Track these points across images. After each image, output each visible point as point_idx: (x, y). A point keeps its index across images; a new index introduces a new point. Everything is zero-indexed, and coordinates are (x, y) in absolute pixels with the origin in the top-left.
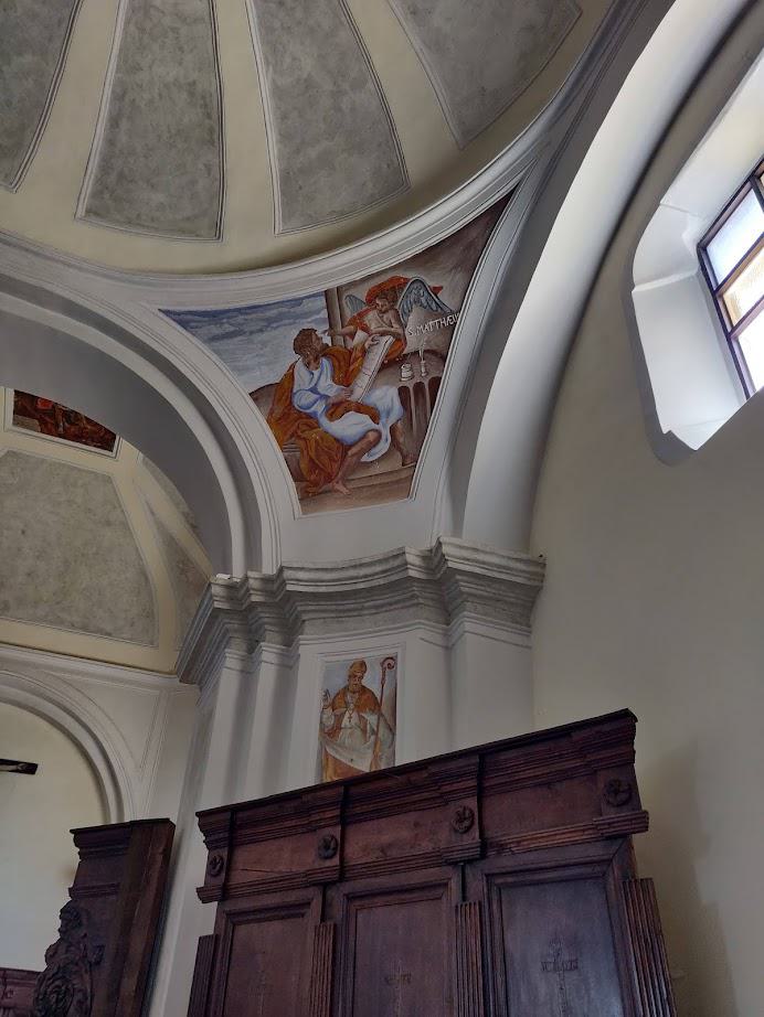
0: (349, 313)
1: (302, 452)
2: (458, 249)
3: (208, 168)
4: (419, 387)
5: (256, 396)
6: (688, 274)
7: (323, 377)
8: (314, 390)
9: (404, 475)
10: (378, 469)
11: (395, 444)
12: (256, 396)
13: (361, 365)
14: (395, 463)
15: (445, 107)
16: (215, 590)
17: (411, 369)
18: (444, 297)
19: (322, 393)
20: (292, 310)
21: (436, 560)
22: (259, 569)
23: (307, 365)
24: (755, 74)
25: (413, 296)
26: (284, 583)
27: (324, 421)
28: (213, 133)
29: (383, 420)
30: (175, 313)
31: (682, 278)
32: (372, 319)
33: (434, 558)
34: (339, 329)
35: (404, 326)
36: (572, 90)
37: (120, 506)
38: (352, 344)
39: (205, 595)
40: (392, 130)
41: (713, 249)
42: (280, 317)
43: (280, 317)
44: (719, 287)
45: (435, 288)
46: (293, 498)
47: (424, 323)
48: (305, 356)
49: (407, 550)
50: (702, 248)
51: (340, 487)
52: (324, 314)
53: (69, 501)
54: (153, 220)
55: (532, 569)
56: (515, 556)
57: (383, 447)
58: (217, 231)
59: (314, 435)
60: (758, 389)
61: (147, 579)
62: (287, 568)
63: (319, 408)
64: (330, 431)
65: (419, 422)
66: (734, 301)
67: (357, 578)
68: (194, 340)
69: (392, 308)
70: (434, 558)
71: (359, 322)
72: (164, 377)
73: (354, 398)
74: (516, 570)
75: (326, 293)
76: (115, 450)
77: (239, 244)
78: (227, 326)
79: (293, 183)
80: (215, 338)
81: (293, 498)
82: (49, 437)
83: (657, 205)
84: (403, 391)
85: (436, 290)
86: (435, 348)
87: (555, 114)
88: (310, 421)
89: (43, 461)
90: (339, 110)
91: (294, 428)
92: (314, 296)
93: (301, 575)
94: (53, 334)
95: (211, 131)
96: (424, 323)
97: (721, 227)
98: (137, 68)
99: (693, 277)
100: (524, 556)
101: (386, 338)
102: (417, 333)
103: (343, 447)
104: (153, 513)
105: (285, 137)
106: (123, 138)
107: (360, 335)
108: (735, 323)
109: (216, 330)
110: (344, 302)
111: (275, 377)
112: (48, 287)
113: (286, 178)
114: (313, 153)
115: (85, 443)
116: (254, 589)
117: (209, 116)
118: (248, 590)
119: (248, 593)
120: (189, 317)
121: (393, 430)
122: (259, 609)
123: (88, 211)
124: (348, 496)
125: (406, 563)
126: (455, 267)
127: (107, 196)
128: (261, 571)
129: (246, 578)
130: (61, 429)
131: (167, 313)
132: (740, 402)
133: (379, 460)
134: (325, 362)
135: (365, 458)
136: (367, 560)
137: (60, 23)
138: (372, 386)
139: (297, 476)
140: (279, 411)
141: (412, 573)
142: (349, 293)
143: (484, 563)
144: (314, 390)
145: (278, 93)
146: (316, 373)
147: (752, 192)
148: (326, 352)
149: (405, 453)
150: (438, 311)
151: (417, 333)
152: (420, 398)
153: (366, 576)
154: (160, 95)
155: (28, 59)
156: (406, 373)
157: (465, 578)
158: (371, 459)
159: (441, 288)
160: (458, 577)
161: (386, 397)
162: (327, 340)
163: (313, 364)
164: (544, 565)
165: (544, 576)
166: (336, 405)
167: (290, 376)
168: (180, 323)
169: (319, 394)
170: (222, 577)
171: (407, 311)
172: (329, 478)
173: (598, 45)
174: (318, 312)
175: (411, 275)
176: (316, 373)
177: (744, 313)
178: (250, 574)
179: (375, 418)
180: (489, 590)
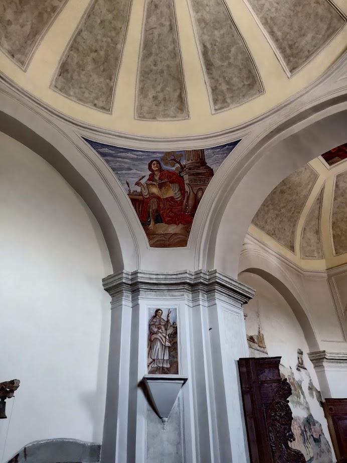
94: (318, 124)
123: (291, 71)
127: (291, 59)
137: (231, 28)
155: (233, 50)
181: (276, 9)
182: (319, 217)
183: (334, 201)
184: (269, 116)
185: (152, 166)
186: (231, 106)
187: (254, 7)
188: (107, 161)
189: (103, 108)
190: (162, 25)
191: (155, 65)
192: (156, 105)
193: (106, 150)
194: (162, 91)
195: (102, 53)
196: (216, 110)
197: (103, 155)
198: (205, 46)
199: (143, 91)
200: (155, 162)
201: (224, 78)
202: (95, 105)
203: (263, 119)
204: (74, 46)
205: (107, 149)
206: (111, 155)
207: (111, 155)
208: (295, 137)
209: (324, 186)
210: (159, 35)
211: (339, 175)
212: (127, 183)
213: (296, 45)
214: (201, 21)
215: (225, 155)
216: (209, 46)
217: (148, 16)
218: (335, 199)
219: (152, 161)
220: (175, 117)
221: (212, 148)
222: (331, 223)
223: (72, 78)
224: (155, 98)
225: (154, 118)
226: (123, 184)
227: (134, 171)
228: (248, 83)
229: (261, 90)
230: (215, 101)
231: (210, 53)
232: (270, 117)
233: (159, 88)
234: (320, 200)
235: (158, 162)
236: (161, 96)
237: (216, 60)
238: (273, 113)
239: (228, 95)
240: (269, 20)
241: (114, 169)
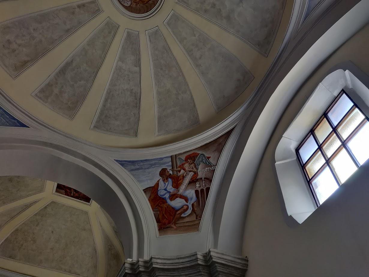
0: (179, 164)
1: (160, 212)
3: (135, 114)
4: (202, 190)
5: (145, 191)
6: (293, 159)
7: (169, 185)
8: (165, 190)
9: (197, 222)
10: (187, 220)
11: (193, 210)
12: (145, 191)
13: (182, 181)
14: (193, 218)
15: (211, 100)
16: (127, 265)
17: (200, 184)
18: (211, 160)
19: (168, 190)
20: (160, 162)
21: (208, 258)
22: (143, 258)
23: (164, 181)
24: (310, 101)
25: (200, 159)
26: (152, 264)
27: (168, 201)
28: (137, 103)
29: (189, 201)
30: (119, 161)
31: (291, 160)
32: (186, 166)
33: (207, 256)
34: (175, 169)
35: (197, 169)
36: (254, 97)
37: (90, 223)
38: (179, 174)
39: (123, 266)
40: (195, 106)
41: (301, 151)
42: (155, 164)
43: (155, 164)
44: (310, 180)
45: (208, 157)
46: (156, 228)
48: (163, 178)
49: (198, 253)
50: (297, 150)
51: (173, 226)
52: (170, 163)
53: (71, 220)
54: (115, 130)
55: (244, 262)
56: (238, 257)
57: (189, 212)
58: (136, 134)
59: (165, 206)
60: (321, 203)
61: (96, 252)
62: (154, 258)
63: (167, 196)
64: (171, 204)
65: (202, 203)
66: (309, 170)
67: (179, 263)
68: (125, 170)
69: (193, 163)
70: (207, 256)
71: (182, 167)
72: (123, 194)
73: (179, 193)
74: (237, 262)
75: (171, 157)
76: (90, 203)
77: (142, 140)
78: (137, 166)
80: (132, 170)
81: (156, 228)
82: (68, 197)
83: (282, 137)
84: (197, 192)
85: (209, 158)
86: (208, 177)
87: (249, 104)
88: (164, 200)
89: (64, 205)
91: (157, 203)
92: (167, 157)
93: (159, 261)
94: (78, 167)
95: (136, 104)
96: (204, 168)
97: (303, 145)
99: (295, 160)
100: (240, 257)
101: (191, 173)
102: (202, 172)
103: (174, 210)
104: (101, 226)
107: (182, 171)
108: (310, 178)
109: (133, 167)
110: (177, 159)
111: (152, 184)
112: (79, 151)
113: (160, 118)
115: (80, 200)
116: (141, 266)
117: (136, 99)
118: (139, 266)
119: (138, 267)
120: (124, 162)
121: (193, 205)
122: (142, 274)
123: (94, 127)
124: (176, 229)
125: (197, 258)
126: (215, 151)
128: (143, 259)
129: (138, 261)
130: (72, 194)
131: (117, 161)
132: (315, 208)
133: (187, 216)
134: (170, 180)
135: (183, 215)
136: (183, 256)
137: (94, 73)
138: (186, 189)
139: (158, 221)
140: (152, 197)
141: (200, 262)
142: (179, 157)
143: (226, 259)
144: (165, 190)
145: (159, 93)
146: (167, 183)
147: (312, 135)
148: (170, 176)
149: (197, 214)
150: (209, 165)
151: (202, 172)
152: (202, 195)
153: (182, 263)
154: (121, 93)
155: (82, 82)
156: (198, 185)
157: (219, 265)
158: (185, 216)
159: (210, 157)
160: (216, 265)
161: (191, 193)
162: (171, 172)
163: (166, 180)
164: (247, 261)
165: (248, 265)
166: (174, 195)
167: (157, 184)
168: (121, 164)
169: (167, 191)
170: (129, 260)
171: (198, 164)
172: (169, 223)
173: (260, 88)
174: (168, 163)
175: (200, 152)
176: (167, 183)
177: (306, 161)
178: (140, 259)
179: (186, 200)
180: (228, 270)
181: (118, 94)
182: (12, 218)
183: (34, 215)
184: (61, 134)
187: (112, 80)
194: (19, 45)
196: (36, 95)
203: (55, 132)
208: (59, 160)
209: (38, 201)
211: (54, 202)
215: (8, 124)
218: (36, 215)
220: (6, 67)
221: (5, 111)
222: (16, 227)
229: (72, 117)
230: (42, 91)
232: (60, 135)
233: (19, 42)
234: (27, 207)
238: (63, 135)
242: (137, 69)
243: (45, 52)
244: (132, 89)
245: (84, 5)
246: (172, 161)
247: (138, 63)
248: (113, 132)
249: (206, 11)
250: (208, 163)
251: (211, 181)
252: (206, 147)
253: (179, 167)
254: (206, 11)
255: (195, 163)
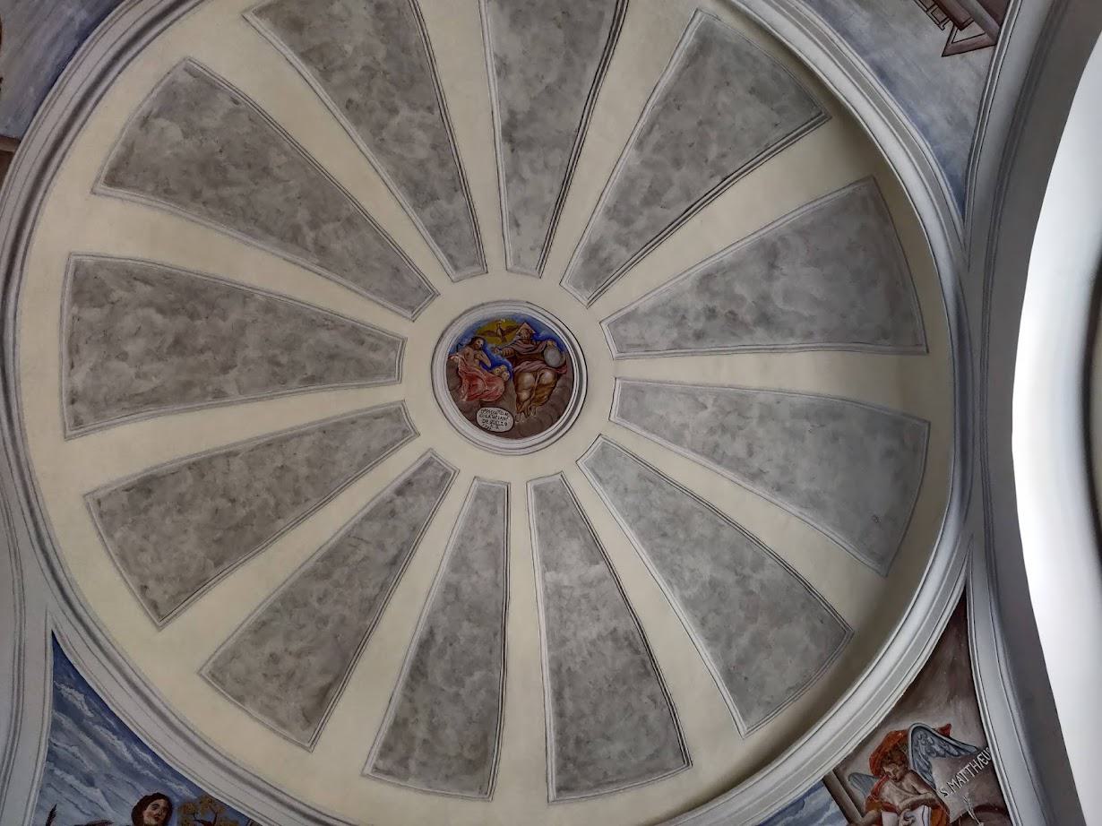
0: (862, 796)
2: (943, 676)
28: (648, 666)
35: (932, 788)
47: (953, 775)
71: (876, 800)
77: (711, 765)
79: (736, 677)
85: (945, 731)
90: (752, 593)
95: (643, 663)
98: (564, 641)
105: (712, 639)
106: (570, 707)
110: (849, 784)
113: (730, 676)
114: (744, 641)
117: (637, 652)
126: (951, 697)
127: (570, 766)
145: (690, 604)
150: (961, 755)
155: (477, 675)
175: (906, 725)
185: (149, 809)
186: (411, 782)
188: (56, 726)
189: (154, 606)
190: (381, 546)
191: (320, 600)
192: (265, 675)
193: (77, 698)
194: (299, 655)
195: (242, 512)
197: (60, 704)
198: (431, 633)
199: (260, 629)
200: (161, 802)
201: (432, 715)
202: (144, 588)
204: (200, 467)
205: (81, 697)
206: (77, 718)
207: (77, 718)
210: (365, 558)
212: (52, 815)
213: (590, 747)
214: (452, 592)
216: (439, 639)
217: (368, 517)
219: (158, 796)
223: (146, 510)
224: (274, 658)
225: (240, 699)
226: (39, 807)
227: (95, 793)
228: (470, 757)
229: (486, 789)
230: (386, 750)
231: (433, 651)
235: (169, 808)
236: (288, 663)
237: (437, 671)
239: (418, 753)
240: (564, 670)
241: (52, 756)
242: (600, 568)
243: (362, 638)
244: (615, 630)
245: (409, 483)
246: (836, 797)
247: (596, 550)
248: (617, 782)
249: (699, 336)
250: (953, 750)
251: (1003, 811)
252: (913, 697)
253: (869, 808)
254: (699, 336)
255: (912, 767)
